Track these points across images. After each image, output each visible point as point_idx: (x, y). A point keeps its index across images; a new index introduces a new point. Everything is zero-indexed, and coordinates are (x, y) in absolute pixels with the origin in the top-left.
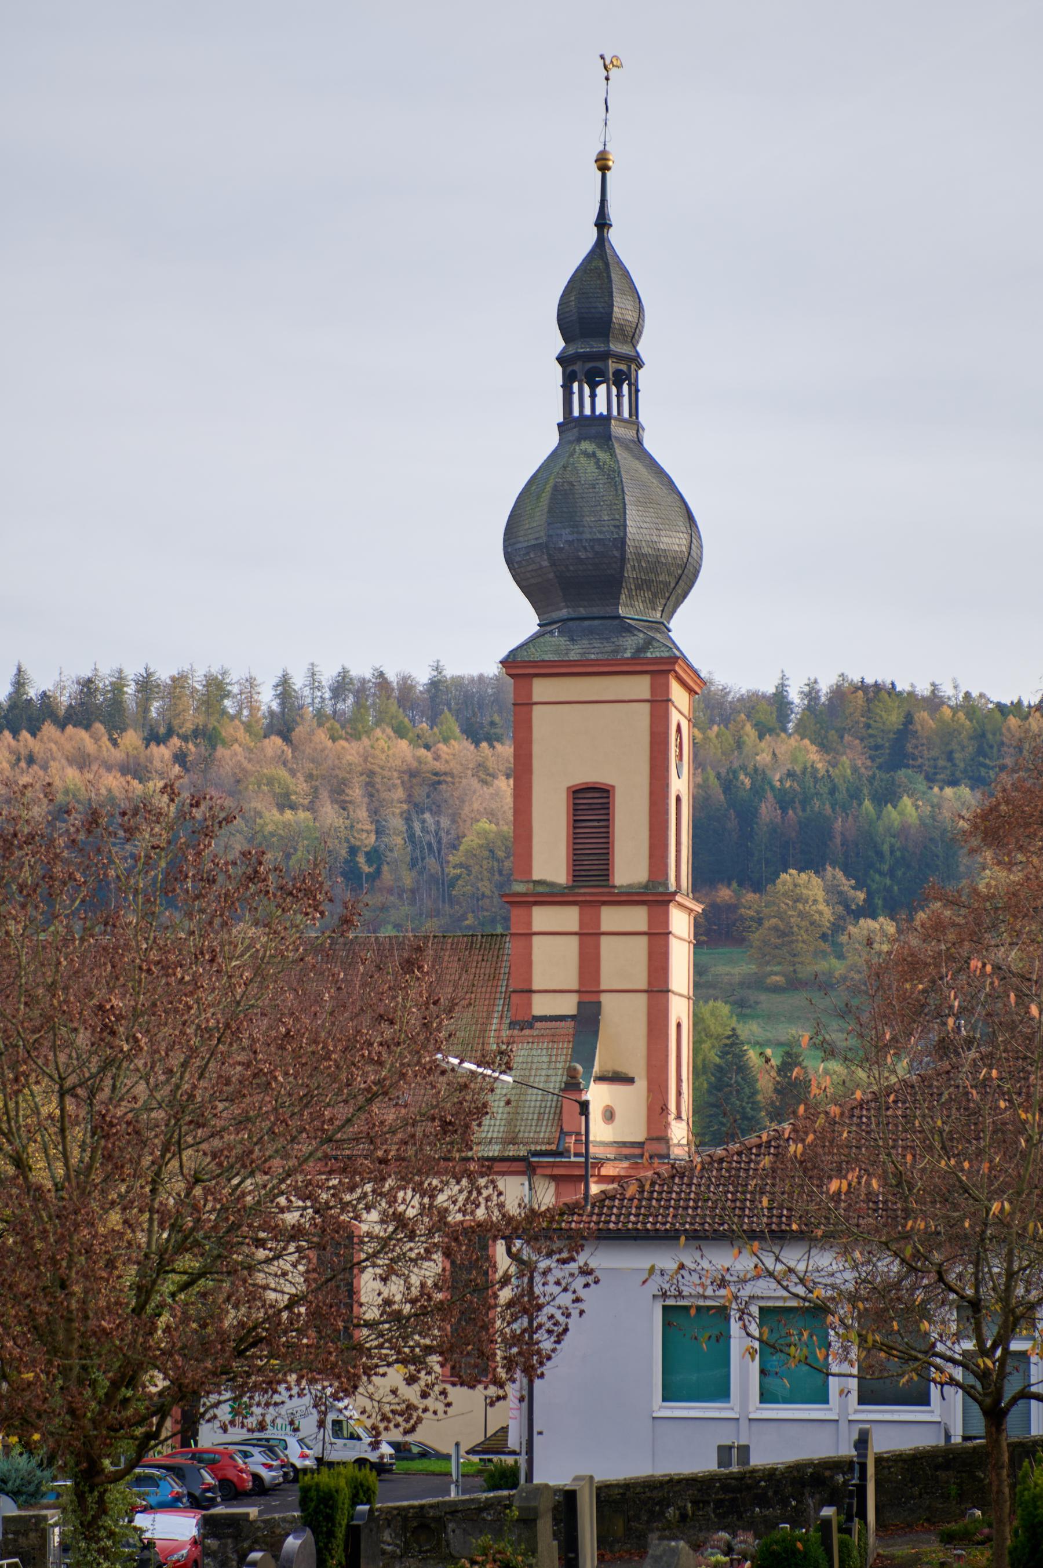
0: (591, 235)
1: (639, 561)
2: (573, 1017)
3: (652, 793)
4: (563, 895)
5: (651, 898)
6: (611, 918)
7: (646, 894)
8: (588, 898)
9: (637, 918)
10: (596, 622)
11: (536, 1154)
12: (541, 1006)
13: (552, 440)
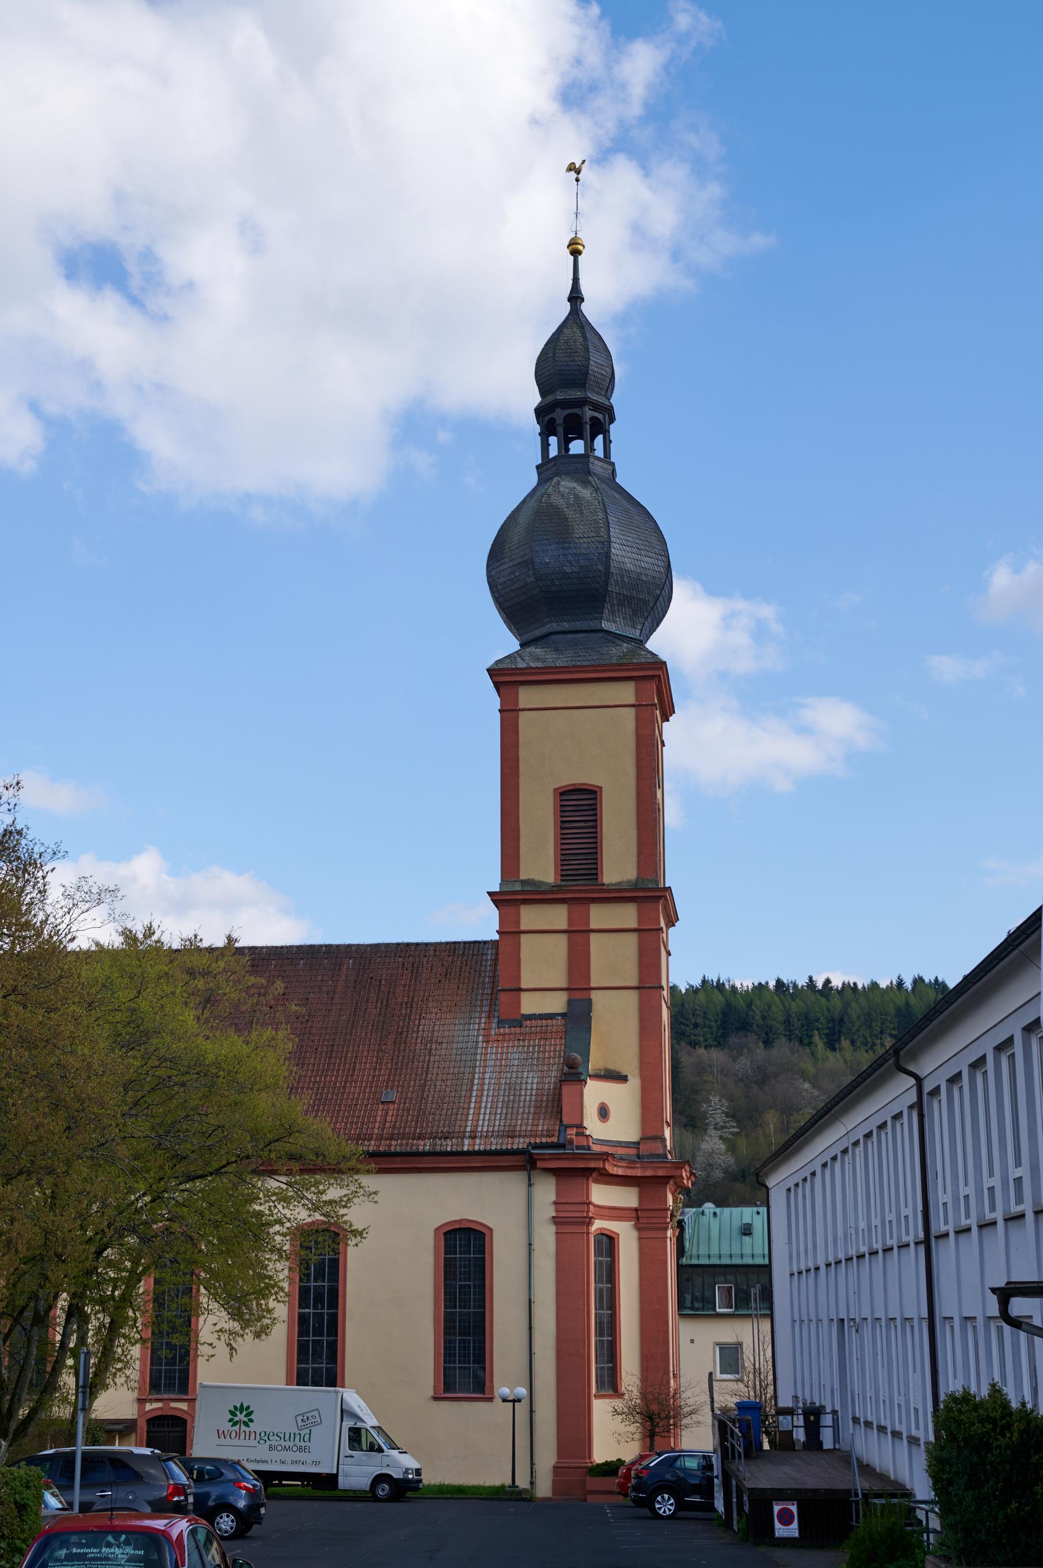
0: (567, 308)
1: (622, 576)
2: (563, 1015)
3: (639, 793)
4: (552, 892)
5: (641, 894)
6: (599, 916)
7: (637, 890)
8: (578, 895)
9: (627, 915)
10: (580, 635)
11: (536, 1146)
12: (530, 1005)
13: (533, 479)
